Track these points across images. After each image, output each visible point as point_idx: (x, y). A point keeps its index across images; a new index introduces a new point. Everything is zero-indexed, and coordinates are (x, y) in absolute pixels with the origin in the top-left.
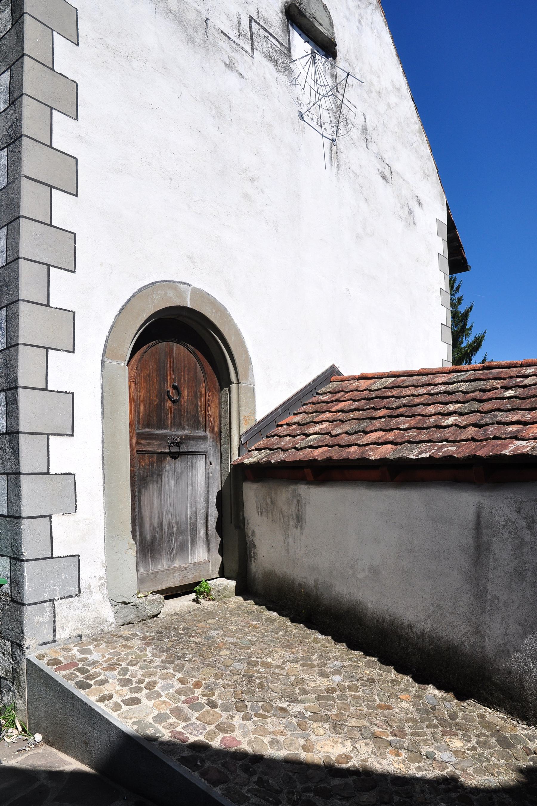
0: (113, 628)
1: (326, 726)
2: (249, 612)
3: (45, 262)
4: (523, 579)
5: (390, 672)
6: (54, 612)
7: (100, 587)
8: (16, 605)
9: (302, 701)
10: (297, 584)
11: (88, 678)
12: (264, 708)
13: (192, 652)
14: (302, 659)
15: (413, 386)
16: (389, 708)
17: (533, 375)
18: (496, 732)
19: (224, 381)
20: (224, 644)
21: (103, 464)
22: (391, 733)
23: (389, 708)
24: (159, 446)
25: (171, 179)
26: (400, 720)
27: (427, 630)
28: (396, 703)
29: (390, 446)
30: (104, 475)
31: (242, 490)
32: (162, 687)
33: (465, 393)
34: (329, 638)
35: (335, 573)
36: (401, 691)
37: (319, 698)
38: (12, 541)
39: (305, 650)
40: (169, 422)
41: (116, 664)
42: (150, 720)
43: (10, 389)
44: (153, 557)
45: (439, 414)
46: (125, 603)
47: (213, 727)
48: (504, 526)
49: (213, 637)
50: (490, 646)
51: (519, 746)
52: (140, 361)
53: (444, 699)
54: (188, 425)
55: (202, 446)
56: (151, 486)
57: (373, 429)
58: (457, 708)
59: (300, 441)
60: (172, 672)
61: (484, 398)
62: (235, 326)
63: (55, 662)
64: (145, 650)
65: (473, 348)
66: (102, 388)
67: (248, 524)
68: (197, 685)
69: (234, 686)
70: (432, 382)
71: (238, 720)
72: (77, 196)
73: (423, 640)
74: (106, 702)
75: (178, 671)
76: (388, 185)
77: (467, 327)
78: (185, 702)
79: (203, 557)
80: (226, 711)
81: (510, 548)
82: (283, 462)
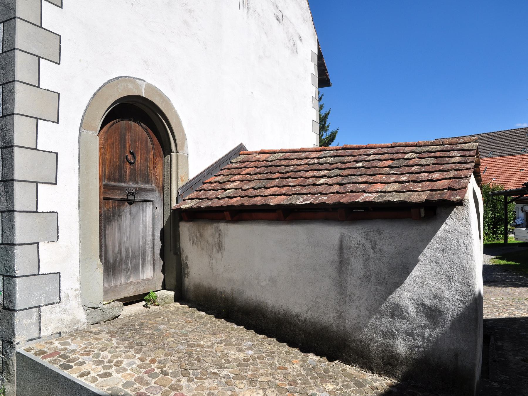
0: (85, 327)
1: (245, 382)
2: (185, 313)
3: (36, 54)
4: (369, 281)
5: (284, 347)
6: (40, 315)
7: (76, 296)
8: (8, 312)
9: (227, 368)
10: (218, 292)
11: (69, 361)
12: (201, 373)
13: (147, 340)
14: (225, 341)
15: (297, 159)
16: (285, 368)
17: (373, 154)
18: (353, 378)
19: (167, 150)
20: (170, 334)
21: (79, 206)
22: (288, 384)
23: (285, 368)
24: (119, 195)
25: (132, 4)
26: (293, 376)
27: (308, 318)
28: (290, 365)
29: (283, 196)
30: (80, 214)
31: (179, 227)
32: (127, 364)
33: (331, 164)
34: (243, 327)
35: (245, 283)
36: (292, 358)
37: (238, 366)
38: (6, 262)
39: (226, 336)
40: (127, 178)
41: (90, 351)
42: (120, 386)
43: (6, 147)
44: (114, 275)
45: (315, 177)
46: (94, 308)
47: (167, 388)
48: (358, 248)
49: (161, 330)
50: (349, 325)
51: (368, 386)
52: (106, 133)
53: (320, 362)
54: (140, 181)
55: (151, 196)
56: (113, 223)
57: (271, 186)
58: (329, 367)
59: (220, 194)
60: (133, 353)
61: (343, 167)
62: (175, 112)
63: (42, 353)
64: (111, 340)
65: (330, 140)
66: (79, 151)
67: (183, 251)
68: (153, 361)
69: (180, 359)
70: (309, 157)
71: (184, 382)
72: (61, 8)
73: (306, 324)
74: (85, 377)
75: (138, 353)
76: (280, 24)
77: (326, 125)
78: (144, 373)
79: (150, 275)
80: (175, 377)
81: (361, 261)
82: (210, 207)
